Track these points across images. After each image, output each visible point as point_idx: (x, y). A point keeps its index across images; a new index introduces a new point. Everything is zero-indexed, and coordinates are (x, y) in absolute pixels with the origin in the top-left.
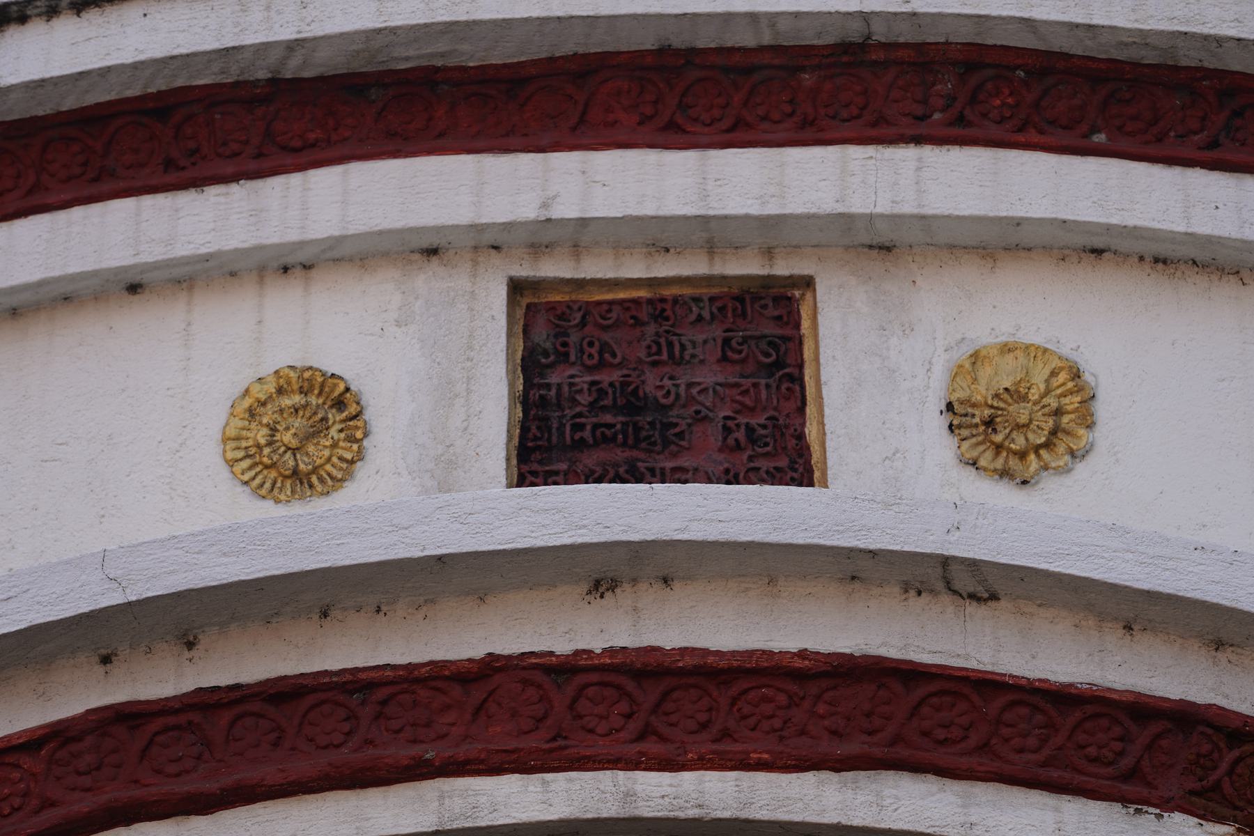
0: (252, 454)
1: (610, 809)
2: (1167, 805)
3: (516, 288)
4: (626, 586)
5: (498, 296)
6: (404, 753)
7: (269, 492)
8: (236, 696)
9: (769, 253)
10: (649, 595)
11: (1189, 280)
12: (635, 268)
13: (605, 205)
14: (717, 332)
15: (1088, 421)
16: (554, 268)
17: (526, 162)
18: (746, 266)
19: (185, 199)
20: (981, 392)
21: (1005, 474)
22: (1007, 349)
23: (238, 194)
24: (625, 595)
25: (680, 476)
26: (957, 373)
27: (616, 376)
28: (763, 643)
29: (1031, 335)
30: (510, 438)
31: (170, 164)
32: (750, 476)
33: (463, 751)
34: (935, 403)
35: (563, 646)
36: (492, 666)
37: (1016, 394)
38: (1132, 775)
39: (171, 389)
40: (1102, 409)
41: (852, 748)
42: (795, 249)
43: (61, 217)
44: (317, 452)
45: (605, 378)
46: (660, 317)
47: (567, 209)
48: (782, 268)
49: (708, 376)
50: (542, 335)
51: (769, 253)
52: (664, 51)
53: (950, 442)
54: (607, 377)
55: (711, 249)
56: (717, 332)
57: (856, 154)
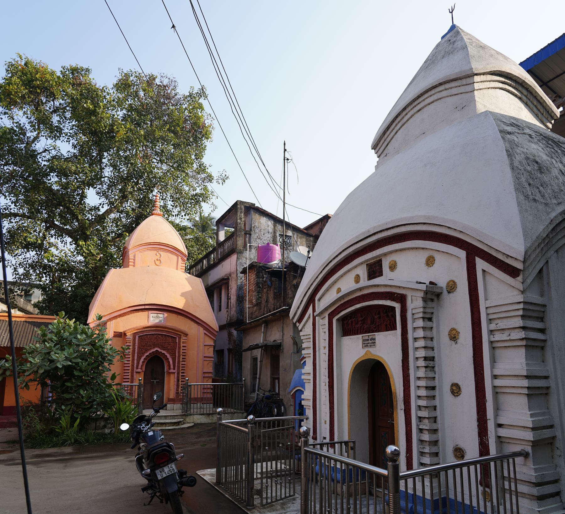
16: (368, 263)
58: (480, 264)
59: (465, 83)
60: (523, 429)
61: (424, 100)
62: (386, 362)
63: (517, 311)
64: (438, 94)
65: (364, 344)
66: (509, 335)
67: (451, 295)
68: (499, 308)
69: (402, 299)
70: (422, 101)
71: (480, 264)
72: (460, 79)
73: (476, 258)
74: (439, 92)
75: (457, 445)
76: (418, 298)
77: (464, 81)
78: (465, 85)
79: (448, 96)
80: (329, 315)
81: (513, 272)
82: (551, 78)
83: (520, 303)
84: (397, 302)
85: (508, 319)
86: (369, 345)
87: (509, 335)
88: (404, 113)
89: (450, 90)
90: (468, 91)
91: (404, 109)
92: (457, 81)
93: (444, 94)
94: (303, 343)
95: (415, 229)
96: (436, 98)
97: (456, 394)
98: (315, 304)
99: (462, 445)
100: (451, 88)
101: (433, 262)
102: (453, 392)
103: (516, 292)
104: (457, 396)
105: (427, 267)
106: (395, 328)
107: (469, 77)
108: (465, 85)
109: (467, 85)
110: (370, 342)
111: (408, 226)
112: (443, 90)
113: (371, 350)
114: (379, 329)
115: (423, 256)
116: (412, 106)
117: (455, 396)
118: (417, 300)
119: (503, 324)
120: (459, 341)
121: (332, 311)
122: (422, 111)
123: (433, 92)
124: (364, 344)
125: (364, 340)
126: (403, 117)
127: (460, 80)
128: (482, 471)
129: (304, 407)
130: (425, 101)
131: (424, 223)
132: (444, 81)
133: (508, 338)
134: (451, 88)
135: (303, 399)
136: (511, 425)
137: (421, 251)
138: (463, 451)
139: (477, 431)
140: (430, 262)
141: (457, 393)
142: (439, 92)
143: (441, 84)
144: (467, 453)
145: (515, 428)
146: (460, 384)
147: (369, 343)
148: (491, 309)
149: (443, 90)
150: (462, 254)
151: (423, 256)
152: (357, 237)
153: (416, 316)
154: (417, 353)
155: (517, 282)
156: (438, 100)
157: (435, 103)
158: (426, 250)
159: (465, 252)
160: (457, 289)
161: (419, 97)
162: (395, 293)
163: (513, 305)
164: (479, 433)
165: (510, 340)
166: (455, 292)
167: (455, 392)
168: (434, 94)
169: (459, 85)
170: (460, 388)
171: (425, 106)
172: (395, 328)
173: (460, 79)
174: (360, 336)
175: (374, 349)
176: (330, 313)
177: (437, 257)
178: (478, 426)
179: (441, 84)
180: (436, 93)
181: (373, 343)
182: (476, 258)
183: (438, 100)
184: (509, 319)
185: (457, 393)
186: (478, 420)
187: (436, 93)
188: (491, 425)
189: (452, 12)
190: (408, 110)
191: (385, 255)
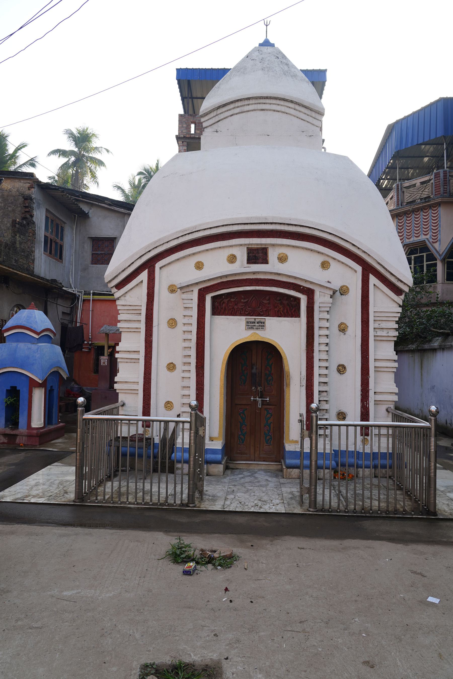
1: (254, 289)
2: (291, 290)
3: (247, 248)
4: (120, 343)
5: (246, 249)
9: (265, 245)
12: (256, 247)
13: (254, 242)
14: (261, 251)
15: (287, 259)
16: (250, 246)
18: (264, 246)
19: (224, 241)
20: (280, 257)
21: (281, 263)
22: (282, 253)
24: (255, 274)
25: (258, 263)
26: (278, 255)
27: (254, 255)
28: (255, 468)
30: (190, 240)
31: (223, 239)
32: (343, 508)
33: (245, 285)
34: (277, 257)
35: (251, 278)
36: (247, 279)
37: (282, 257)
40: (288, 258)
44: (233, 260)
46: (257, 250)
48: (266, 247)
49: (261, 255)
50: (249, 251)
51: (265, 245)
53: (278, 260)
57: (272, 239)
58: (373, 280)
59: (314, 116)
60: (390, 394)
61: (270, 104)
62: (279, 345)
63: (394, 318)
64: (286, 108)
65: (248, 326)
67: (343, 297)
69: (310, 293)
71: (373, 280)
72: (311, 110)
73: (370, 275)
74: (288, 107)
78: (313, 117)
79: (294, 116)
80: (200, 290)
81: (397, 291)
82: (198, 96)
84: (303, 294)
86: (254, 327)
89: (298, 112)
90: (315, 124)
91: (249, 99)
93: (292, 111)
94: (119, 314)
96: (283, 110)
97: (342, 373)
98: (154, 271)
99: (344, 410)
100: (300, 111)
102: (339, 371)
103: (396, 305)
104: (343, 374)
105: (321, 269)
106: (298, 315)
107: (318, 113)
108: (313, 117)
109: (315, 118)
110: (256, 324)
111: (313, 230)
114: (268, 314)
115: (320, 259)
117: (341, 374)
118: (324, 296)
119: (384, 325)
120: (347, 333)
121: (207, 287)
122: (265, 112)
123: (282, 103)
124: (248, 326)
125: (247, 322)
126: (244, 105)
127: (310, 111)
128: (77, 470)
129: (117, 391)
130: (271, 105)
131: (330, 234)
132: (297, 101)
133: (387, 335)
134: (300, 111)
135: (116, 383)
138: (345, 414)
139: (360, 398)
140: (325, 265)
142: (288, 107)
143: (292, 102)
144: (348, 415)
145: (385, 394)
147: (255, 326)
148: (377, 313)
149: (292, 108)
150: (359, 269)
151: (321, 259)
152: (248, 218)
154: (320, 339)
155: (400, 299)
157: (280, 113)
159: (361, 267)
160: (349, 293)
161: (267, 98)
163: (394, 313)
165: (388, 336)
166: (347, 295)
170: (345, 368)
171: (270, 110)
172: (298, 315)
174: (244, 318)
175: (263, 332)
176: (204, 288)
178: (361, 395)
179: (292, 102)
181: (262, 325)
182: (370, 275)
184: (387, 322)
185: (343, 372)
186: (362, 391)
188: (371, 393)
189: (267, 26)
190: (251, 102)
191: (273, 245)
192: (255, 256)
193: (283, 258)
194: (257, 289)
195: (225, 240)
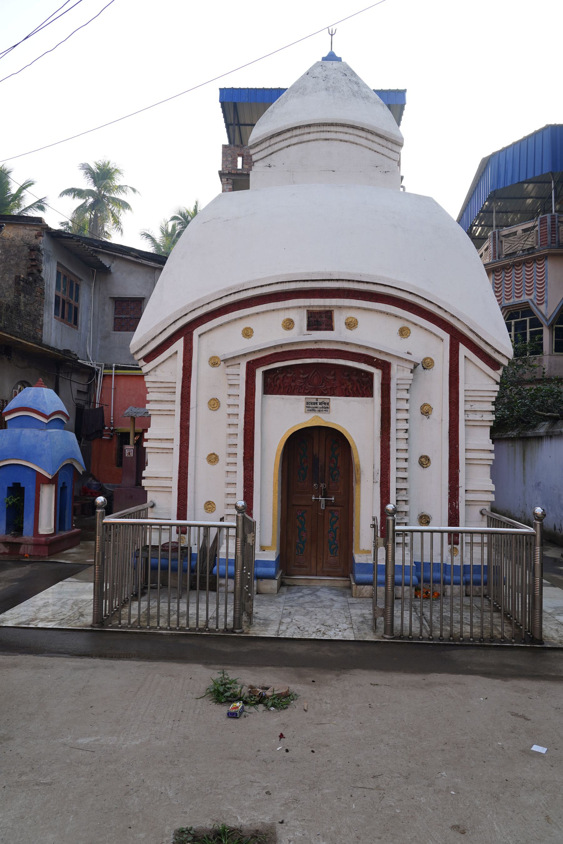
0: (284, 326)
1: (316, 362)
2: (362, 362)
3: (307, 310)
5: (306, 311)
6: (300, 357)
7: (286, 330)
8: (286, 352)
9: (330, 308)
10: (320, 343)
11: (259, 824)
13: (316, 304)
14: (325, 315)
15: (357, 324)
17: (308, 300)
18: (328, 309)
19: (278, 303)
20: (348, 321)
21: (350, 329)
22: (350, 317)
23: (283, 302)
24: (318, 343)
29: (353, 316)
34: (344, 322)
35: (313, 348)
36: (307, 349)
37: (351, 322)
38: (359, 360)
39: (229, 220)
40: (359, 323)
41: (336, 357)
42: (332, 307)
43: (267, 304)
44: (290, 326)
45: (315, 319)
47: (312, 304)
50: (309, 315)
51: (330, 308)
52: (321, 289)
54: (315, 319)
55: (325, 307)
56: (325, 315)
57: (338, 299)
58: (463, 350)
61: (336, 132)
62: (346, 432)
65: (309, 407)
66: (482, 416)
68: (476, 392)
69: (385, 367)
70: (334, 132)
71: (463, 350)
72: (387, 139)
73: (460, 344)
74: (358, 136)
75: (423, 513)
76: (406, 369)
77: (390, 145)
78: (389, 149)
79: (366, 147)
80: (248, 363)
81: (494, 364)
83: (496, 391)
85: (480, 402)
87: (482, 416)
88: (307, 130)
90: (392, 157)
91: (309, 126)
92: (382, 139)
94: (148, 393)
95: (398, 295)
97: (425, 466)
99: (427, 512)
100: (373, 141)
101: (408, 334)
104: (426, 467)
105: (400, 337)
106: (370, 394)
107: (396, 144)
108: (389, 149)
110: (319, 406)
112: (363, 137)
113: (321, 415)
114: (333, 393)
115: (398, 325)
116: (319, 129)
117: (424, 467)
119: (477, 406)
120: (431, 416)
123: (351, 131)
124: (309, 407)
129: (146, 489)
131: (411, 293)
133: (481, 419)
134: (373, 141)
135: (144, 478)
136: (473, 490)
137: (394, 319)
138: (429, 518)
139: (448, 497)
140: (404, 332)
141: (426, 464)
142: (358, 136)
143: (363, 129)
145: (478, 492)
146: (430, 456)
149: (363, 137)
150: (446, 337)
151: (399, 324)
152: (308, 274)
153: (401, 387)
154: (398, 424)
155: (497, 375)
156: (353, 143)
158: (399, 319)
159: (449, 335)
160: (434, 367)
161: (332, 125)
162: (374, 358)
163: (490, 392)
164: (449, 499)
165: (483, 421)
166: (431, 370)
167: (425, 463)
168: (350, 134)
169: (383, 144)
170: (429, 460)
172: (370, 394)
173: (387, 139)
174: (303, 397)
176: (253, 360)
177: (412, 328)
178: (449, 493)
179: (363, 129)
180: (353, 134)
181: (326, 407)
182: (460, 344)
183: (353, 143)
184: (481, 403)
185: (426, 464)
186: (450, 488)
187: (353, 134)
188: (461, 492)
189: (332, 35)
190: (312, 129)
191: (340, 307)
192: (317, 321)
193: (351, 323)
194: (319, 362)
195: (279, 301)
